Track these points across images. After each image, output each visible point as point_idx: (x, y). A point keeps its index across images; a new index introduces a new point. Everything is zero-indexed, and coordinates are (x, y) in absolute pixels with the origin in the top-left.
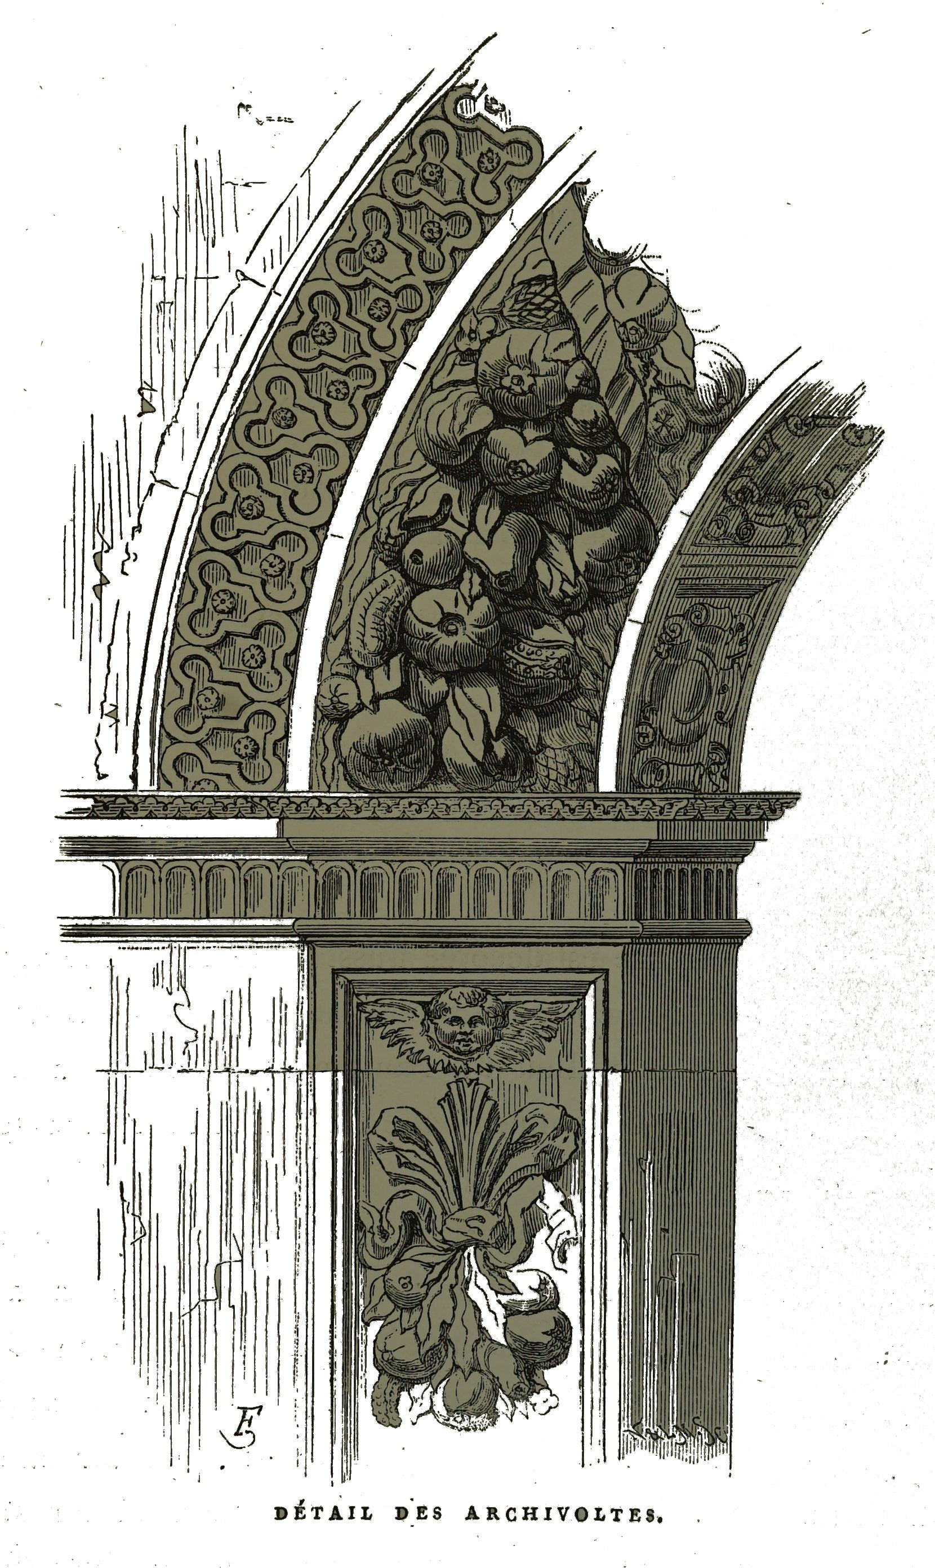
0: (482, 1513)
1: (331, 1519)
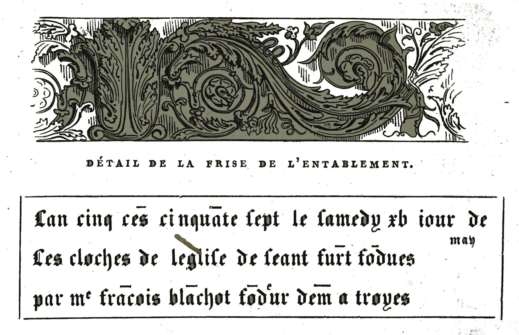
0: (340, 164)
1: (117, 166)
